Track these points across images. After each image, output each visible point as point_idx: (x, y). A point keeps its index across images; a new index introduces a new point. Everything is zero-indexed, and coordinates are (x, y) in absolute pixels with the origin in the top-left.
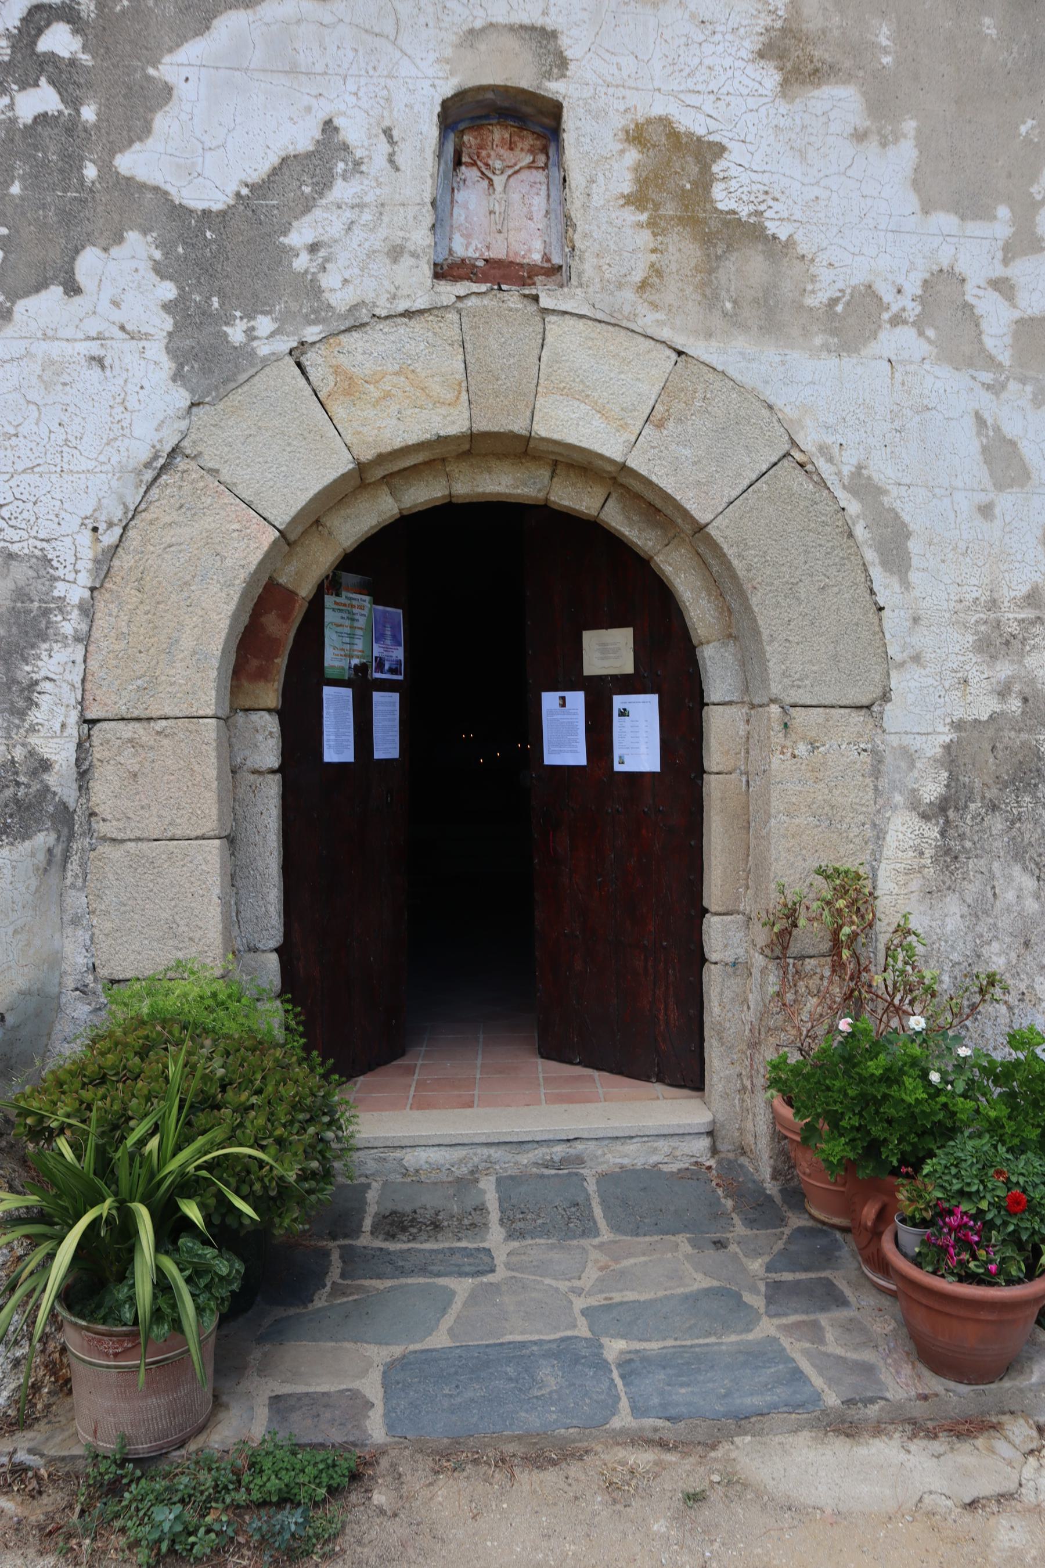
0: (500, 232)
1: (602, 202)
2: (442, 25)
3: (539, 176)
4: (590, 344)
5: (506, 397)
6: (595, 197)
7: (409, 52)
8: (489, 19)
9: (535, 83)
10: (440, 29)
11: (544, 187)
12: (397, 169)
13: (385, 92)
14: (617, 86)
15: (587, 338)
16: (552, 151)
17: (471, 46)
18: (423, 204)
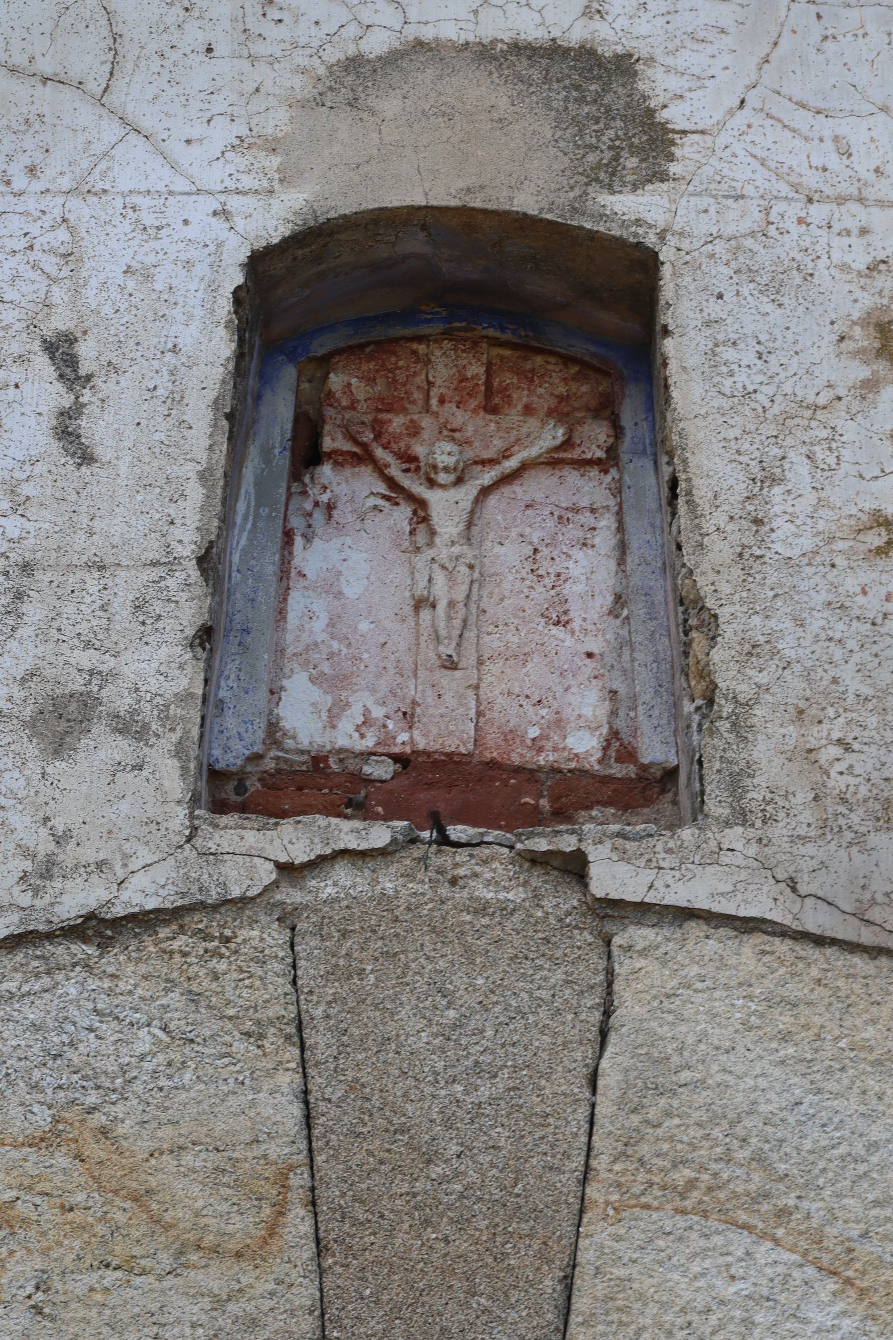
0: (450, 664)
1: (807, 543)
2: (259, 48)
3: (590, 488)
4: (784, 1020)
5: (462, 1223)
6: (783, 528)
7: (146, 124)
8: (411, 33)
9: (564, 199)
10: (252, 59)
11: (607, 522)
12: (86, 458)
13: (63, 234)
14: (841, 200)
15: (770, 1001)
16: (630, 412)
17: (353, 104)
18: (171, 564)
